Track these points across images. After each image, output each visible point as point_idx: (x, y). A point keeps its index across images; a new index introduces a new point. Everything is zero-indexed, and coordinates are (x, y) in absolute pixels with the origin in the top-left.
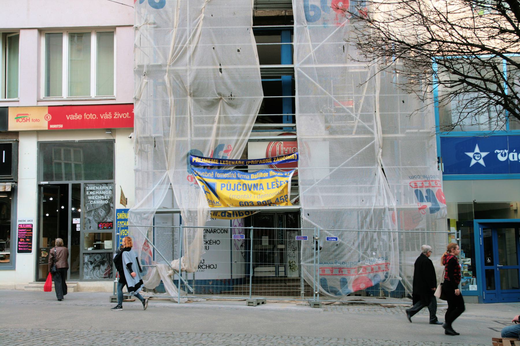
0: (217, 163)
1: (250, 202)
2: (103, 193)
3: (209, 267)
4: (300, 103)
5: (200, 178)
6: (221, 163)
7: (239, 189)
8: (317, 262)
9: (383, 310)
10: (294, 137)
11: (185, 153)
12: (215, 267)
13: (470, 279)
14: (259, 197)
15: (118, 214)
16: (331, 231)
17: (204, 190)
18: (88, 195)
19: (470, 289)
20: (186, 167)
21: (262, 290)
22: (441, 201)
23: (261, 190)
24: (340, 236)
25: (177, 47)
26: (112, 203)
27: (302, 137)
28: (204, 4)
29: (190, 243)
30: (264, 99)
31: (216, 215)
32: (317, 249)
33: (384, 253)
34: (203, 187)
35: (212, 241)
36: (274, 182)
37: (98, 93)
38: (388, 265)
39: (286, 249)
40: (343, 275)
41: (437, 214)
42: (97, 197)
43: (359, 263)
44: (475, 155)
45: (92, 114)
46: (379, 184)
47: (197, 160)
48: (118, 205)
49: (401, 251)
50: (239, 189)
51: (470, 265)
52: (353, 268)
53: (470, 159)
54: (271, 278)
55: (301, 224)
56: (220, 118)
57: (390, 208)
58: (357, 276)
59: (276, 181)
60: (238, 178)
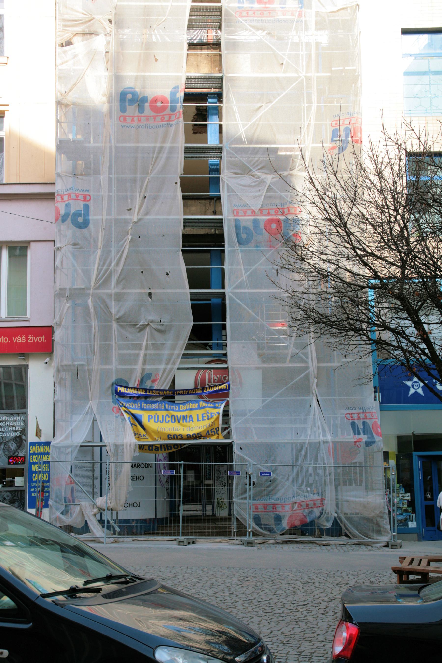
0: (144, 393)
1: (179, 435)
2: (15, 424)
3: (133, 505)
4: (231, 330)
5: (125, 409)
7: (167, 421)
8: (250, 497)
9: (318, 547)
10: (225, 365)
11: (110, 382)
12: (138, 505)
13: (410, 516)
14: (188, 429)
15: (31, 447)
16: (265, 466)
17: (130, 422)
19: (410, 526)
20: (111, 397)
21: (188, 530)
22: (377, 434)
23: (191, 422)
24: (274, 471)
25: (101, 269)
26: (25, 435)
27: (234, 366)
28: (131, 225)
29: (116, 479)
30: (194, 325)
31: (143, 449)
32: (250, 485)
33: (320, 489)
34: (129, 418)
35: (135, 477)
36: (205, 414)
37: (9, 313)
38: (324, 501)
39: (213, 485)
40: (277, 511)
41: (374, 447)
42: (7, 429)
43: (293, 499)
45: (4, 337)
46: (314, 415)
47: (122, 390)
48: (32, 437)
49: (336, 487)
50: (167, 421)
51: (410, 500)
52: (287, 504)
53: (408, 388)
54: (198, 518)
55: (234, 458)
56: (147, 345)
57: (325, 441)
59: (206, 412)
60: (166, 410)
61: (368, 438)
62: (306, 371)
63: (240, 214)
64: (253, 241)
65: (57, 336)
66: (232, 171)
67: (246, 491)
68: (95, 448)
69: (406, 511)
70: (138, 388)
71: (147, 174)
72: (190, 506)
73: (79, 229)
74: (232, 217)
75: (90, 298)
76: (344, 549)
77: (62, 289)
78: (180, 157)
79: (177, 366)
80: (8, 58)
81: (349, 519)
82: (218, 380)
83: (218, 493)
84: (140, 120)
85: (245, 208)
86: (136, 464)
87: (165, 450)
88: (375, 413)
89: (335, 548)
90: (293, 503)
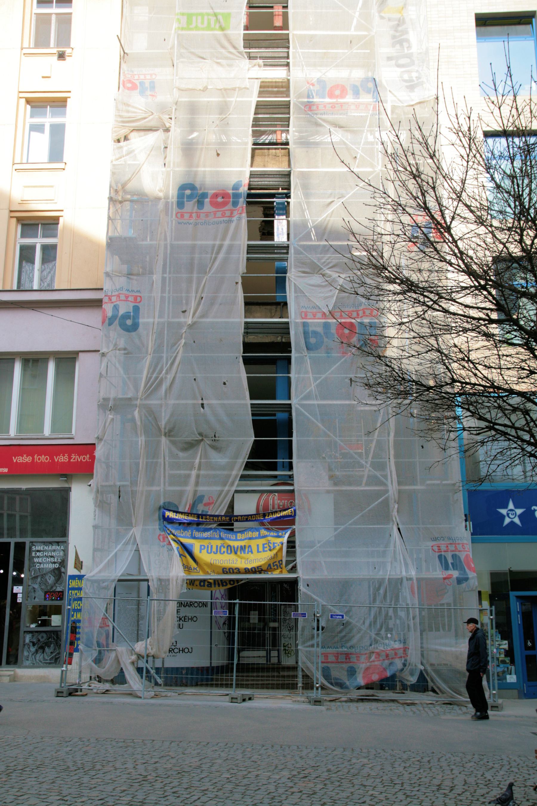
1: (236, 569)
2: (54, 554)
3: (183, 650)
4: (298, 447)
5: (174, 537)
6: (200, 520)
7: (222, 552)
10: (291, 488)
12: (190, 650)
13: (508, 668)
14: (246, 562)
15: (71, 581)
17: (179, 552)
18: (34, 557)
20: (158, 523)
22: (470, 568)
23: (250, 553)
24: (347, 613)
25: (151, 378)
26: (64, 567)
29: (159, 620)
30: (255, 440)
31: (193, 585)
32: (318, 630)
34: (178, 548)
36: (266, 544)
37: (53, 430)
38: (407, 650)
39: (279, 628)
40: (350, 662)
43: (371, 647)
44: (509, 512)
45: (45, 456)
46: (395, 547)
47: (171, 515)
48: (71, 570)
50: (222, 552)
51: (507, 649)
53: (503, 517)
58: (368, 664)
59: (267, 542)
60: (221, 538)
61: (460, 574)
62: (385, 495)
63: (308, 317)
64: (323, 347)
65: (98, 453)
66: (300, 270)
67: (313, 637)
68: (142, 583)
69: (503, 662)
70: (189, 513)
71: (205, 273)
72: (251, 652)
73: (127, 333)
74: (299, 320)
75: (137, 410)
76: (433, 711)
77: (106, 400)
78: (241, 259)
79: (234, 488)
80: (66, 163)
81: (437, 672)
82: (284, 505)
83: (284, 638)
84: (198, 217)
85: (315, 310)
86: (189, 603)
87: (219, 585)
88: (467, 544)
89: (422, 709)
90: (370, 653)
